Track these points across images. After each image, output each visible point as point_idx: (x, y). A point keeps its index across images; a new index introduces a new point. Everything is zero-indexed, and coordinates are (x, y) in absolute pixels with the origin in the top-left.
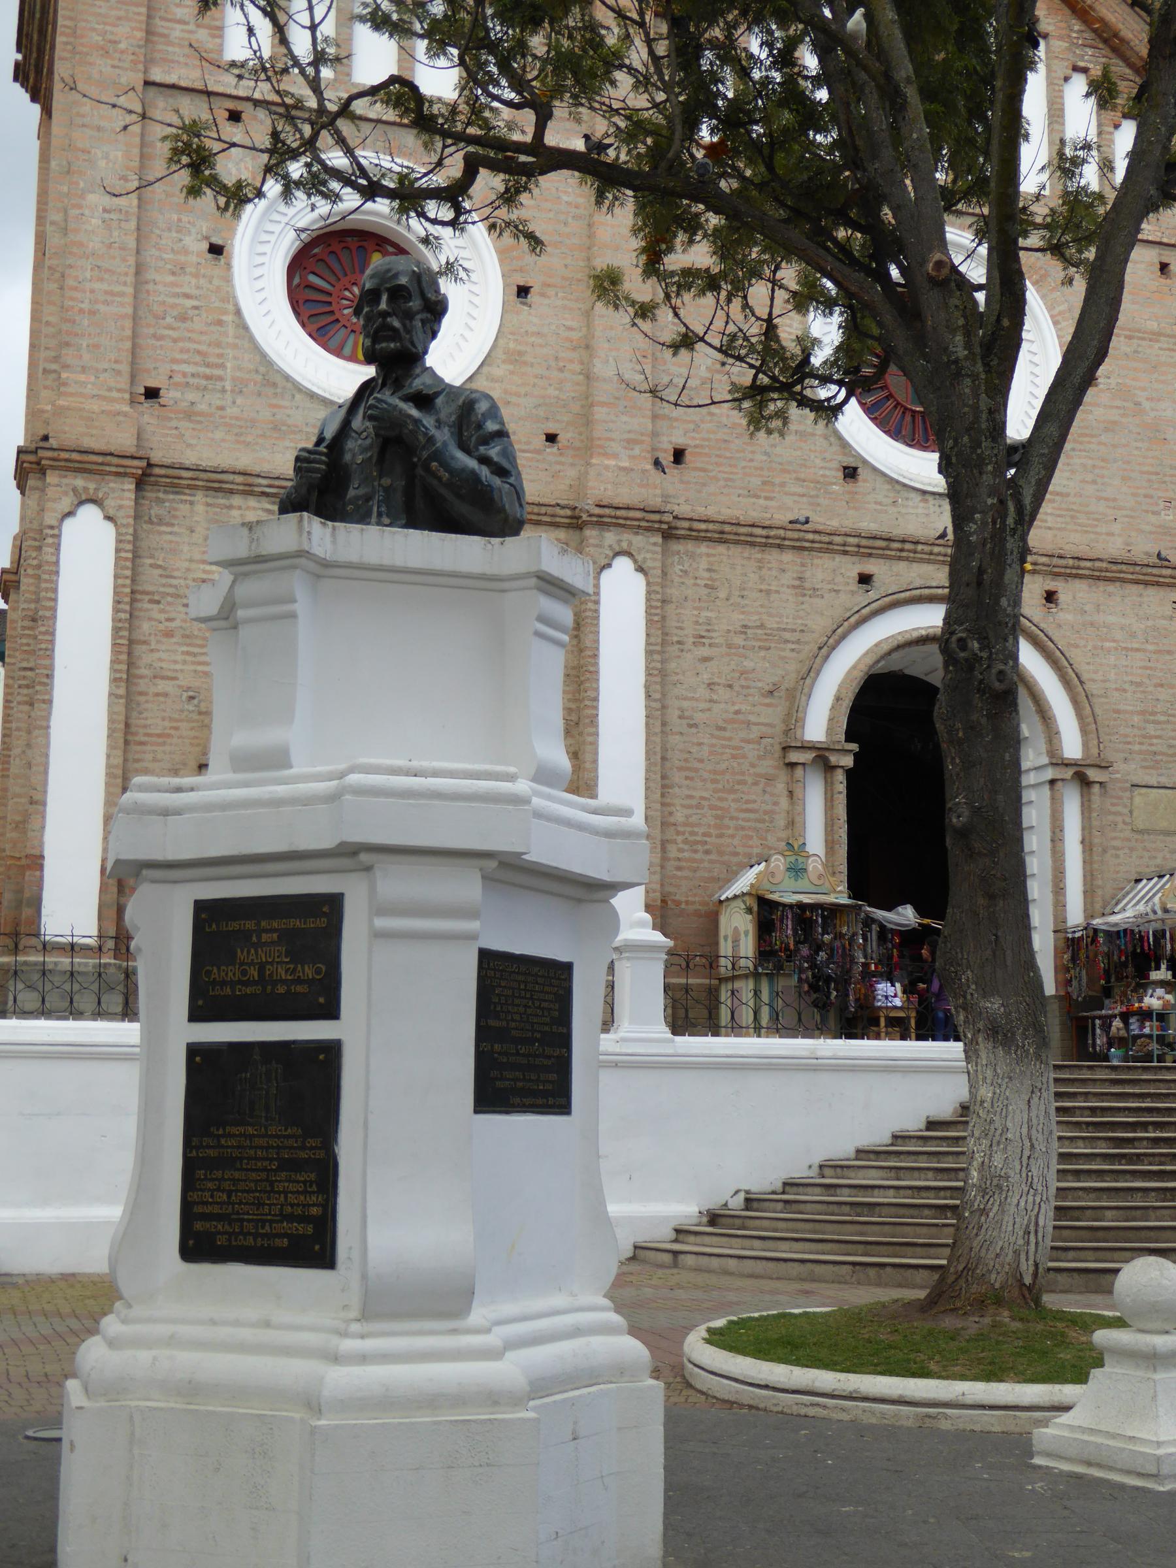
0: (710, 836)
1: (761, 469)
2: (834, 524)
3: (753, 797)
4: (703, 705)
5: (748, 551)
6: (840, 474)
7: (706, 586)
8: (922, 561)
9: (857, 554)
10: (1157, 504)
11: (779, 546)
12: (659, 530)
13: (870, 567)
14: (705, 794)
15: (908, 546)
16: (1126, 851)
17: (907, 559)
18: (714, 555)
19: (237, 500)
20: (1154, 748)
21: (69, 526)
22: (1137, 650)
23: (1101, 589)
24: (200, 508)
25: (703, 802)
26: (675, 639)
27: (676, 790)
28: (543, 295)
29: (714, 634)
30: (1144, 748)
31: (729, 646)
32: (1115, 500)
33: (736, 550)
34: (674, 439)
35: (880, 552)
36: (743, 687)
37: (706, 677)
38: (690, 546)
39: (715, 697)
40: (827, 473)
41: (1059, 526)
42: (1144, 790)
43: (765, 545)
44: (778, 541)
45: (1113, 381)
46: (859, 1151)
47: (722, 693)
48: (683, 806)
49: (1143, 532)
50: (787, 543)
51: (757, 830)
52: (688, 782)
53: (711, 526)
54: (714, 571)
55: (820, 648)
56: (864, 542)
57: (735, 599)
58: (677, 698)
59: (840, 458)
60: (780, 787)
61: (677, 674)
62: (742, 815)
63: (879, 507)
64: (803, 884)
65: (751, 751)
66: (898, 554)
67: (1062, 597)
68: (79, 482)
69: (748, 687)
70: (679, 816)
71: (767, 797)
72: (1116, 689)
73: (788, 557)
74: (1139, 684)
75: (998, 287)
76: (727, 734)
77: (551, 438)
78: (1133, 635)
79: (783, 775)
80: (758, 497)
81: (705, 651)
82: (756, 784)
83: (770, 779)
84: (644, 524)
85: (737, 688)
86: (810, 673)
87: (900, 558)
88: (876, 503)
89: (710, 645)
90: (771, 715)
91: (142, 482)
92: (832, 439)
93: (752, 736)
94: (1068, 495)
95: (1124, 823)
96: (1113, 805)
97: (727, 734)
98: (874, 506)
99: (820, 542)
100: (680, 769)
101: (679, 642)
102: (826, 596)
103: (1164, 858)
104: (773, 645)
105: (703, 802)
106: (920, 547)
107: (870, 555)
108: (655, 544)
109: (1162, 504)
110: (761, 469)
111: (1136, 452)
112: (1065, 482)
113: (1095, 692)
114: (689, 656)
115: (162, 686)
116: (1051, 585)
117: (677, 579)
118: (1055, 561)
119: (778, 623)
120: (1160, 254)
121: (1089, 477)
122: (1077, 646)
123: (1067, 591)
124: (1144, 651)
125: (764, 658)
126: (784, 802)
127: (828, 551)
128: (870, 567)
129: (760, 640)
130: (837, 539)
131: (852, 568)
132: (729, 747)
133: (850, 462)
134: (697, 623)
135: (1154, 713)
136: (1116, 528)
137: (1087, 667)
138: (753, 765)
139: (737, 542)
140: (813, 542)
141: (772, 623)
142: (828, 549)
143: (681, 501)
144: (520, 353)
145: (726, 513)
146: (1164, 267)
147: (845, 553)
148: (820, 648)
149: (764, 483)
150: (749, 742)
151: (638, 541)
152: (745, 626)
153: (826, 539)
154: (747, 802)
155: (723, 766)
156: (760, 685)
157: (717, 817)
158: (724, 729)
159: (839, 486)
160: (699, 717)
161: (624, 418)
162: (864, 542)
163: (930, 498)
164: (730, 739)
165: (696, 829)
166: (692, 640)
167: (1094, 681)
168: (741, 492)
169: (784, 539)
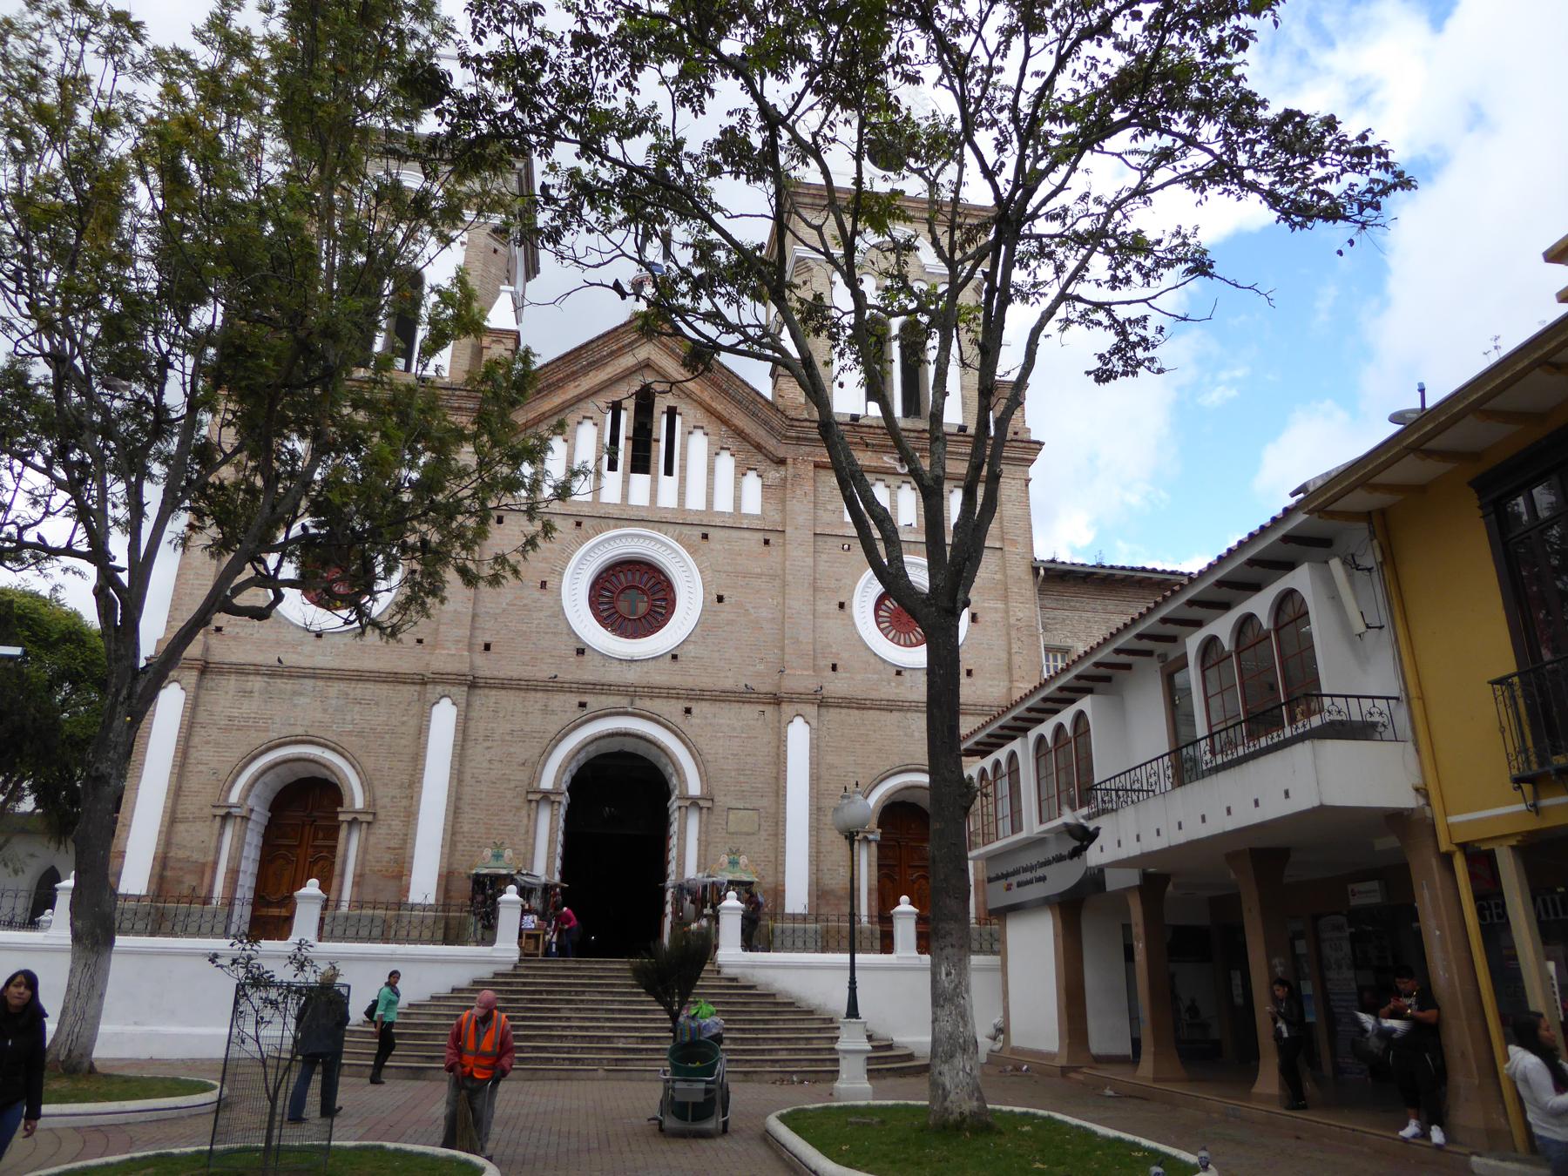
2: (569, 677)
5: (518, 693)
19: (251, 678)
21: (435, 708)
24: (232, 682)
38: (486, 691)
46: (433, 998)
60: (524, 812)
64: (500, 863)
65: (509, 795)
67: (694, 711)
73: (539, 695)
77: (420, 641)
79: (526, 806)
83: (518, 809)
86: (546, 753)
90: (522, 776)
115: (201, 767)
116: (688, 704)
126: (525, 821)
128: (585, 699)
131: (575, 700)
136: (730, 674)
142: (562, 690)
145: (510, 674)
146: (767, 542)
151: (454, 690)
159: (573, 659)
160: (481, 777)
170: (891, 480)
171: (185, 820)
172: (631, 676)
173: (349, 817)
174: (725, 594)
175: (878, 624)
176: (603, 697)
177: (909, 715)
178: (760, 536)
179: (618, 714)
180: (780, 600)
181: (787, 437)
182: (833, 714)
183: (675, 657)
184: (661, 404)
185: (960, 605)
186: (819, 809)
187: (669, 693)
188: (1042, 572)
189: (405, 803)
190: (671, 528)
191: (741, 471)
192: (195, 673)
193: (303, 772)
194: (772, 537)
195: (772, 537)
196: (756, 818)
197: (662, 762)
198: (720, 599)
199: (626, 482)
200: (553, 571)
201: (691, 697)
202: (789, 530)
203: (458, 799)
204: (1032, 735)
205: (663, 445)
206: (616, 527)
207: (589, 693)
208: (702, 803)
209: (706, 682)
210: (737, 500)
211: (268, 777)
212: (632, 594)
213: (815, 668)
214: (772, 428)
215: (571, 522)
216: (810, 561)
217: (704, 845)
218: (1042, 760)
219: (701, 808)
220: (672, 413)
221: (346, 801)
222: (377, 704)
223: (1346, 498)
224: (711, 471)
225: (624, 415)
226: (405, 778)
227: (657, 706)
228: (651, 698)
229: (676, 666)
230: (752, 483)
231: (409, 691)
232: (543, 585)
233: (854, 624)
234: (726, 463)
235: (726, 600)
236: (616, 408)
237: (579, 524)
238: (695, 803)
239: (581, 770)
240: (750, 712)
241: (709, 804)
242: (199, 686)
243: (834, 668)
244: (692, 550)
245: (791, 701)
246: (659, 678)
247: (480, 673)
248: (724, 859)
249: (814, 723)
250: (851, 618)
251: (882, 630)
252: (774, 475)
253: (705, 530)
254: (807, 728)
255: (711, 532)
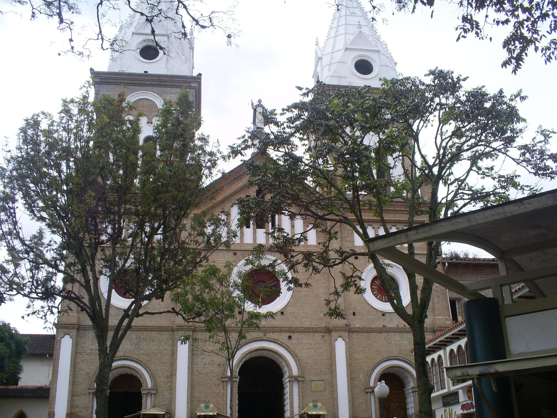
24: (91, 333)
37: (203, 363)
47: (207, 366)
60: (221, 387)
67: (293, 337)
68: (65, 331)
70: (197, 394)
75: (492, 219)
78: (311, 345)
83: (219, 385)
91: (78, 330)
115: (82, 372)
116: (290, 334)
123: (294, 336)
126: (222, 391)
170: (375, 225)
171: (77, 396)
173: (146, 392)
175: (372, 292)
177: (389, 334)
179: (259, 340)
180: (327, 284)
182: (355, 336)
185: (423, 317)
186: (351, 379)
187: (281, 330)
188: (447, 264)
189: (169, 384)
192: (75, 330)
197: (279, 361)
201: (291, 331)
203: (192, 381)
204: (448, 349)
208: (299, 379)
209: (297, 324)
217: (302, 397)
218: (453, 360)
219: (299, 381)
222: (153, 341)
223: (437, 142)
226: (169, 374)
228: (273, 332)
229: (284, 317)
231: (166, 336)
238: (295, 379)
239: (246, 362)
240: (318, 336)
242: (77, 336)
243: (354, 314)
245: (336, 331)
248: (311, 405)
249: (347, 340)
251: (374, 295)
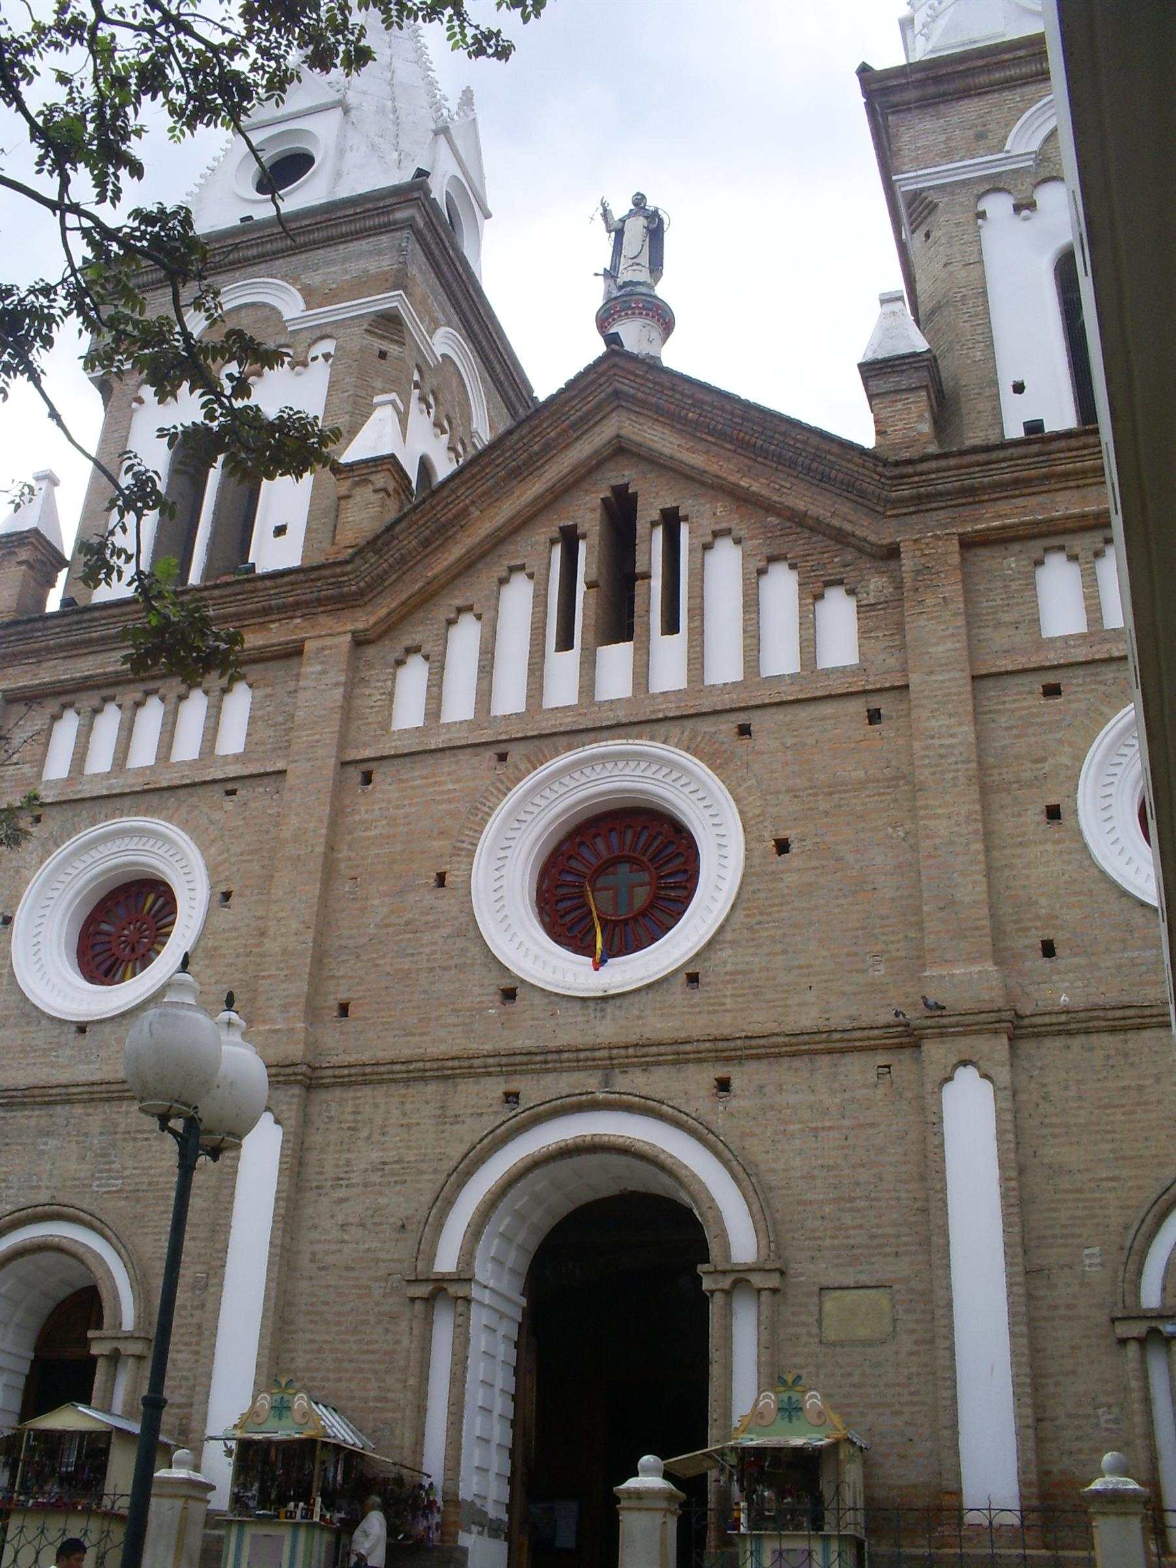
0: (328, 1380)
1: (419, 1007)
3: (376, 1337)
4: (333, 1247)
6: (498, 998)
7: (349, 1128)
8: (570, 1070)
9: (501, 1073)
10: (863, 961)
11: (423, 1079)
12: (296, 1082)
13: (515, 1084)
14: (329, 1338)
15: (550, 1057)
16: (811, 1369)
17: (555, 1070)
18: (359, 1098)
20: (851, 1241)
22: (830, 1128)
23: (785, 1066)
25: (325, 1346)
26: (315, 1184)
27: (300, 1335)
28: (241, 895)
29: (351, 1175)
30: (837, 1242)
31: (366, 1185)
32: (809, 966)
33: (381, 1091)
34: (339, 996)
35: (524, 1067)
36: (375, 1224)
37: (340, 1218)
38: (337, 1093)
39: (346, 1237)
40: (484, 998)
41: (740, 1006)
42: (838, 1293)
43: (409, 1080)
44: (420, 1074)
45: (809, 844)
47: (355, 1233)
48: (305, 1351)
49: (844, 994)
50: (428, 1074)
51: (376, 1372)
52: (312, 1326)
53: (353, 1071)
54: (359, 1113)
55: (449, 1175)
56: (504, 1060)
57: (376, 1137)
58: (311, 1243)
59: (499, 982)
61: (313, 1218)
62: (364, 1357)
63: (536, 1023)
66: (544, 1066)
67: (735, 1084)
69: (380, 1224)
71: (389, 1336)
72: (803, 1177)
73: (432, 1087)
74: (830, 1168)
76: (355, 1274)
78: (826, 1112)
80: (413, 1034)
81: (341, 1193)
82: (379, 1322)
83: (393, 1317)
84: (281, 1078)
85: (369, 1226)
86: (444, 1201)
87: (547, 1071)
88: (533, 1019)
89: (347, 1186)
92: (492, 965)
93: (379, 1274)
94: (752, 971)
95: (809, 1334)
96: (794, 1314)
97: (355, 1274)
98: (530, 1023)
99: (460, 1068)
100: (308, 1313)
101: (317, 1187)
102: (468, 1120)
103: (863, 1374)
104: (408, 1178)
105: (325, 1346)
106: (565, 1056)
107: (515, 1072)
108: (293, 1096)
109: (870, 961)
110: (419, 1007)
111: (837, 910)
112: (748, 959)
113: (774, 1184)
114: (326, 1200)
116: (721, 1071)
117: (322, 1126)
118: (720, 1045)
119: (417, 1155)
120: (867, 702)
121: (778, 948)
122: (753, 1135)
124: (839, 1128)
125: (399, 1193)
127: (470, 1075)
128: (515, 1084)
129: (397, 1175)
130: (476, 1062)
131: (496, 1088)
132: (356, 1287)
133: (507, 983)
134: (337, 1166)
135: (852, 1199)
136: (810, 997)
137: (765, 1156)
138: (378, 1304)
139: (381, 1082)
140: (453, 1068)
141: (410, 1156)
143: (340, 1052)
144: (216, 948)
147: (489, 1074)
148: (449, 1175)
149: (420, 1020)
150: (376, 1279)
152: (384, 1163)
153: (466, 1063)
154: (369, 1343)
155: (349, 1307)
156: (392, 1220)
157: (335, 1360)
158: (353, 1269)
161: (284, 986)
162: (504, 1060)
163: (592, 1004)
164: (357, 1279)
165: (315, 1375)
166: (329, 1183)
167: (773, 1171)
168: (397, 1032)
169: (425, 1070)
172: (607, 1029)
174: (790, 834)
176: (549, 1079)
178: (858, 707)
181: (895, 503)
182: (1050, 1051)
183: (693, 979)
184: (648, 511)
187: (679, 1054)
190: (675, 729)
191: (812, 593)
193: (599, 1181)
194: (883, 703)
195: (883, 703)
196: (885, 1304)
198: (782, 847)
199: (589, 664)
200: (456, 852)
201: (726, 1056)
202: (914, 679)
205: (657, 583)
206: (569, 748)
207: (536, 1065)
209: (760, 1020)
210: (808, 645)
211: (518, 1199)
212: (618, 871)
213: (1001, 955)
214: (862, 494)
215: (490, 754)
216: (966, 731)
220: (671, 521)
221: (107, 1320)
224: (752, 603)
225: (582, 547)
227: (635, 1082)
228: (646, 1067)
230: (839, 614)
232: (441, 879)
233: (1085, 847)
234: (781, 586)
235: (795, 847)
236: (569, 539)
237: (502, 757)
240: (858, 1070)
241: (774, 1281)
243: (1048, 949)
244: (717, 761)
246: (659, 1025)
247: (1027, 1008)
249: (1004, 1075)
250: (1078, 834)
252: (877, 585)
253: (742, 719)
254: (987, 1088)
255: (755, 720)
